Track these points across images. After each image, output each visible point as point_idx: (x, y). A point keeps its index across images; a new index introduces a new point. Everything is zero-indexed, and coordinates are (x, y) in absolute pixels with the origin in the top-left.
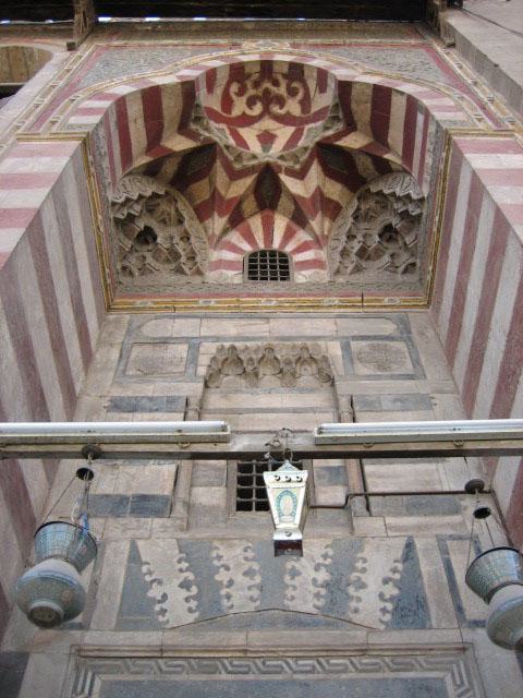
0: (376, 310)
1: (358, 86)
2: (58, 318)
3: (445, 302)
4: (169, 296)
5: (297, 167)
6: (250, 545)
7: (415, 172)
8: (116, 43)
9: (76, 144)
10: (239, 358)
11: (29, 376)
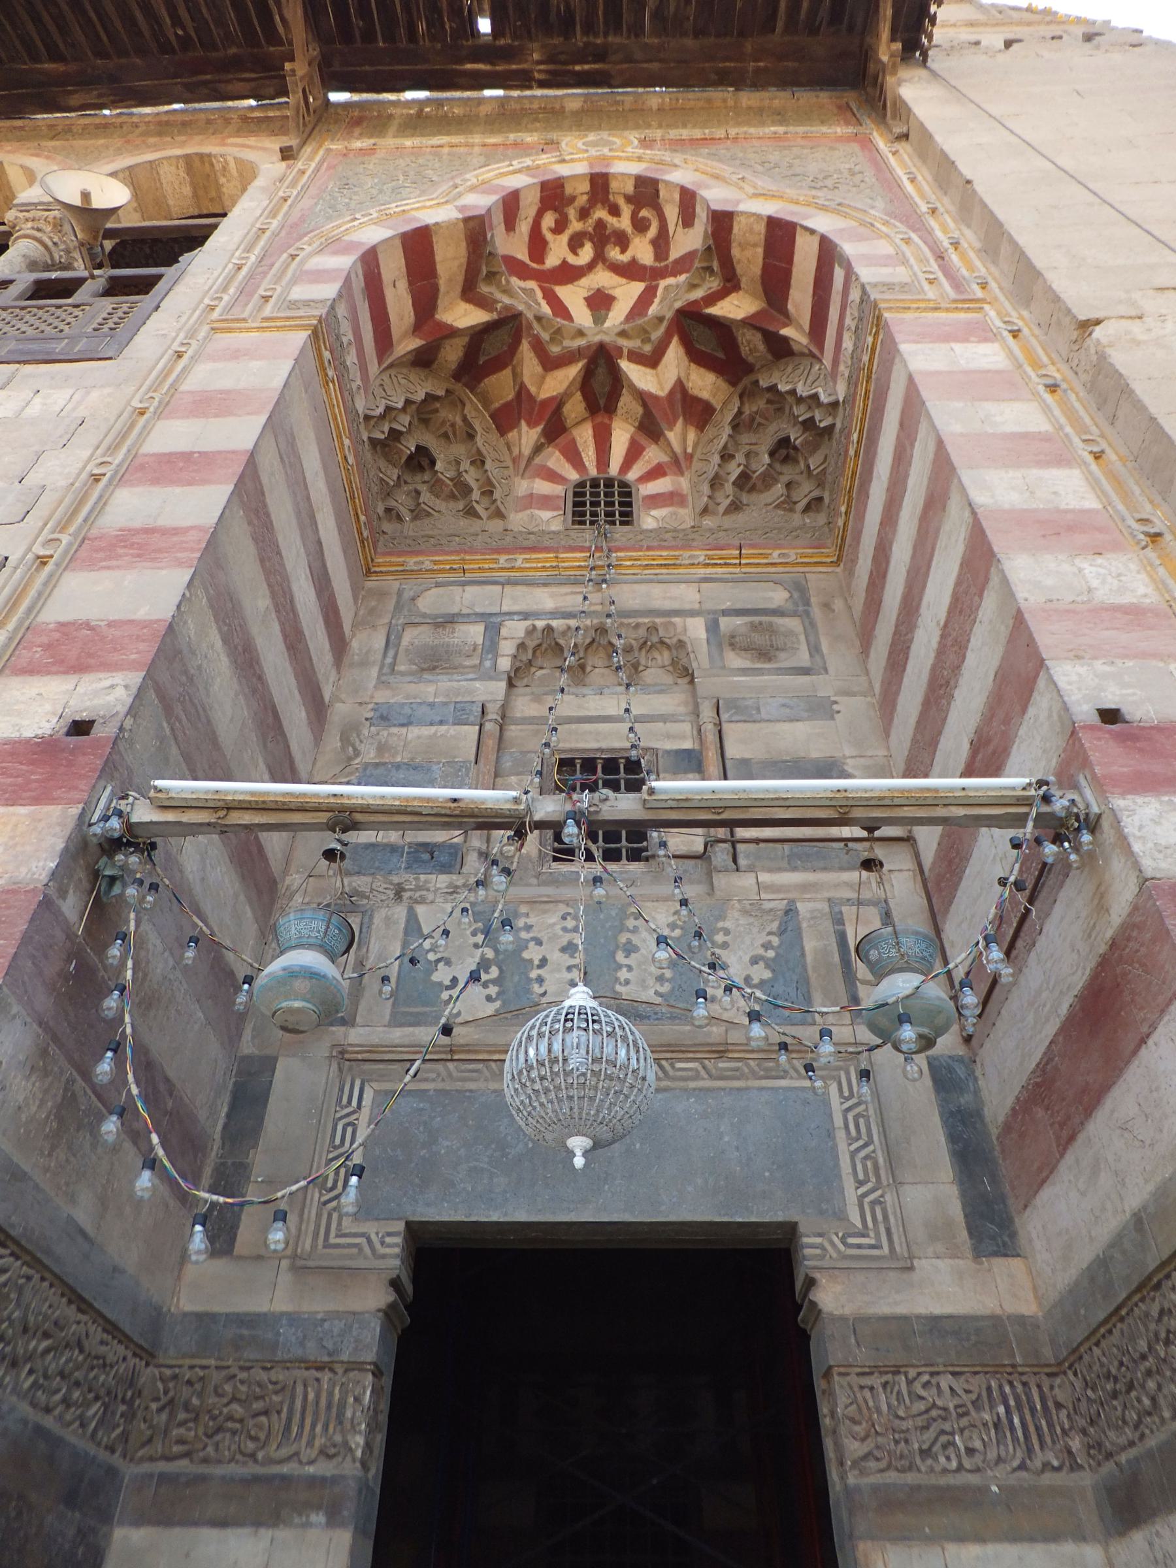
0: (759, 570)
1: (742, 219)
2: (292, 601)
3: (861, 561)
4: (457, 552)
5: (647, 348)
6: (571, 911)
7: (827, 361)
8: (358, 144)
9: (302, 336)
10: (557, 644)
11: (254, 691)
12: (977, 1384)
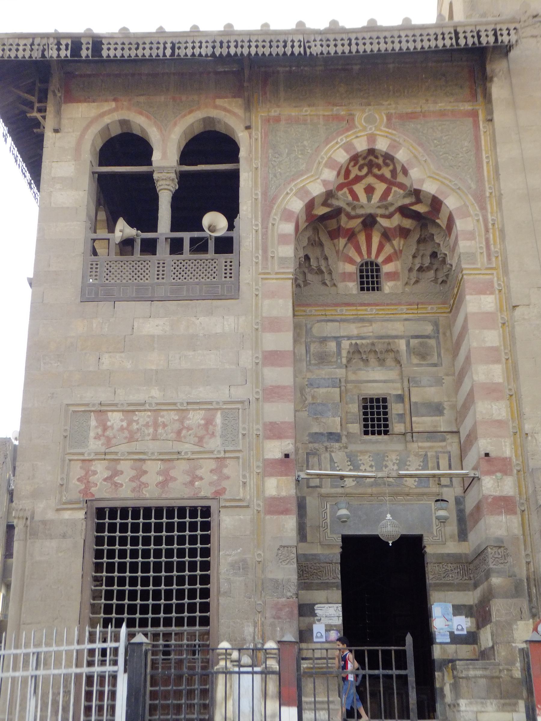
12: (455, 565)
